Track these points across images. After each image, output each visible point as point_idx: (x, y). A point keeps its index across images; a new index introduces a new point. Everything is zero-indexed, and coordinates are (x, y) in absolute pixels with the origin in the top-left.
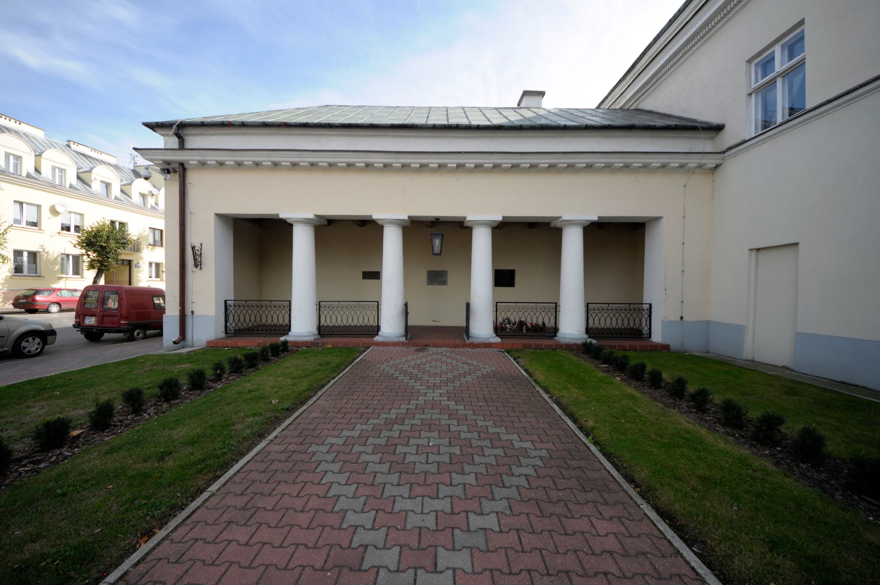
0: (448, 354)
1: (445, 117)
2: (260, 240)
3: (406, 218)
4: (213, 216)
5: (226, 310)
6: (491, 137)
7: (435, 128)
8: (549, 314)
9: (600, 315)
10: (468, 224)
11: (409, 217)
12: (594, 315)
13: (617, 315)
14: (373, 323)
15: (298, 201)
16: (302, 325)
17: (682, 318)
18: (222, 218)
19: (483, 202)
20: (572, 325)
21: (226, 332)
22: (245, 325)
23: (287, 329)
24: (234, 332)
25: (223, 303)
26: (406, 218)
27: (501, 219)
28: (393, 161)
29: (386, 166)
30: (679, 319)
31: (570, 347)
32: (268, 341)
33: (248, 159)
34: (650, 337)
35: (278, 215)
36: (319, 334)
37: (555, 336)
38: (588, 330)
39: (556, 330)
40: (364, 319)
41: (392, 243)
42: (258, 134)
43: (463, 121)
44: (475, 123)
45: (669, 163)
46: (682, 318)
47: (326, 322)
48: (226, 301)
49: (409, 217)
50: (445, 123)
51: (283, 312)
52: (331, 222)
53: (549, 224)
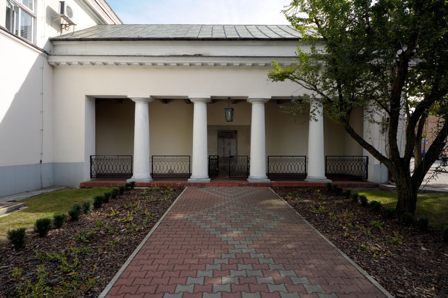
0: (229, 191)
1: (211, 33)
2: (111, 113)
3: (210, 97)
4: (84, 98)
5: (91, 161)
6: (283, 46)
7: (230, 39)
8: (302, 163)
9: (334, 164)
10: (250, 101)
11: (211, 97)
12: (330, 164)
13: (334, 164)
14: (302, 171)
15: (137, 86)
16: (141, 172)
17: (41, 161)
18: (89, 98)
19: (199, 86)
20: (316, 171)
21: (91, 177)
22: (105, 172)
23: (131, 175)
24: (98, 176)
25: (89, 157)
26: (148, 97)
27: (270, 98)
28: (184, 62)
29: (203, 65)
30: (39, 162)
31: (255, 185)
32: (120, 183)
33: (87, 61)
34: (367, 178)
35: (127, 96)
36: (152, 178)
37: (248, 178)
38: (268, 174)
39: (305, 175)
40: (178, 168)
41: (200, 114)
42: (228, 45)
43: (222, 36)
44: (229, 37)
45: (258, 63)
46: (41, 161)
47: (157, 171)
48: (91, 156)
49: (211, 97)
50: (210, 36)
51: (127, 163)
52: (166, 101)
53: (246, 100)
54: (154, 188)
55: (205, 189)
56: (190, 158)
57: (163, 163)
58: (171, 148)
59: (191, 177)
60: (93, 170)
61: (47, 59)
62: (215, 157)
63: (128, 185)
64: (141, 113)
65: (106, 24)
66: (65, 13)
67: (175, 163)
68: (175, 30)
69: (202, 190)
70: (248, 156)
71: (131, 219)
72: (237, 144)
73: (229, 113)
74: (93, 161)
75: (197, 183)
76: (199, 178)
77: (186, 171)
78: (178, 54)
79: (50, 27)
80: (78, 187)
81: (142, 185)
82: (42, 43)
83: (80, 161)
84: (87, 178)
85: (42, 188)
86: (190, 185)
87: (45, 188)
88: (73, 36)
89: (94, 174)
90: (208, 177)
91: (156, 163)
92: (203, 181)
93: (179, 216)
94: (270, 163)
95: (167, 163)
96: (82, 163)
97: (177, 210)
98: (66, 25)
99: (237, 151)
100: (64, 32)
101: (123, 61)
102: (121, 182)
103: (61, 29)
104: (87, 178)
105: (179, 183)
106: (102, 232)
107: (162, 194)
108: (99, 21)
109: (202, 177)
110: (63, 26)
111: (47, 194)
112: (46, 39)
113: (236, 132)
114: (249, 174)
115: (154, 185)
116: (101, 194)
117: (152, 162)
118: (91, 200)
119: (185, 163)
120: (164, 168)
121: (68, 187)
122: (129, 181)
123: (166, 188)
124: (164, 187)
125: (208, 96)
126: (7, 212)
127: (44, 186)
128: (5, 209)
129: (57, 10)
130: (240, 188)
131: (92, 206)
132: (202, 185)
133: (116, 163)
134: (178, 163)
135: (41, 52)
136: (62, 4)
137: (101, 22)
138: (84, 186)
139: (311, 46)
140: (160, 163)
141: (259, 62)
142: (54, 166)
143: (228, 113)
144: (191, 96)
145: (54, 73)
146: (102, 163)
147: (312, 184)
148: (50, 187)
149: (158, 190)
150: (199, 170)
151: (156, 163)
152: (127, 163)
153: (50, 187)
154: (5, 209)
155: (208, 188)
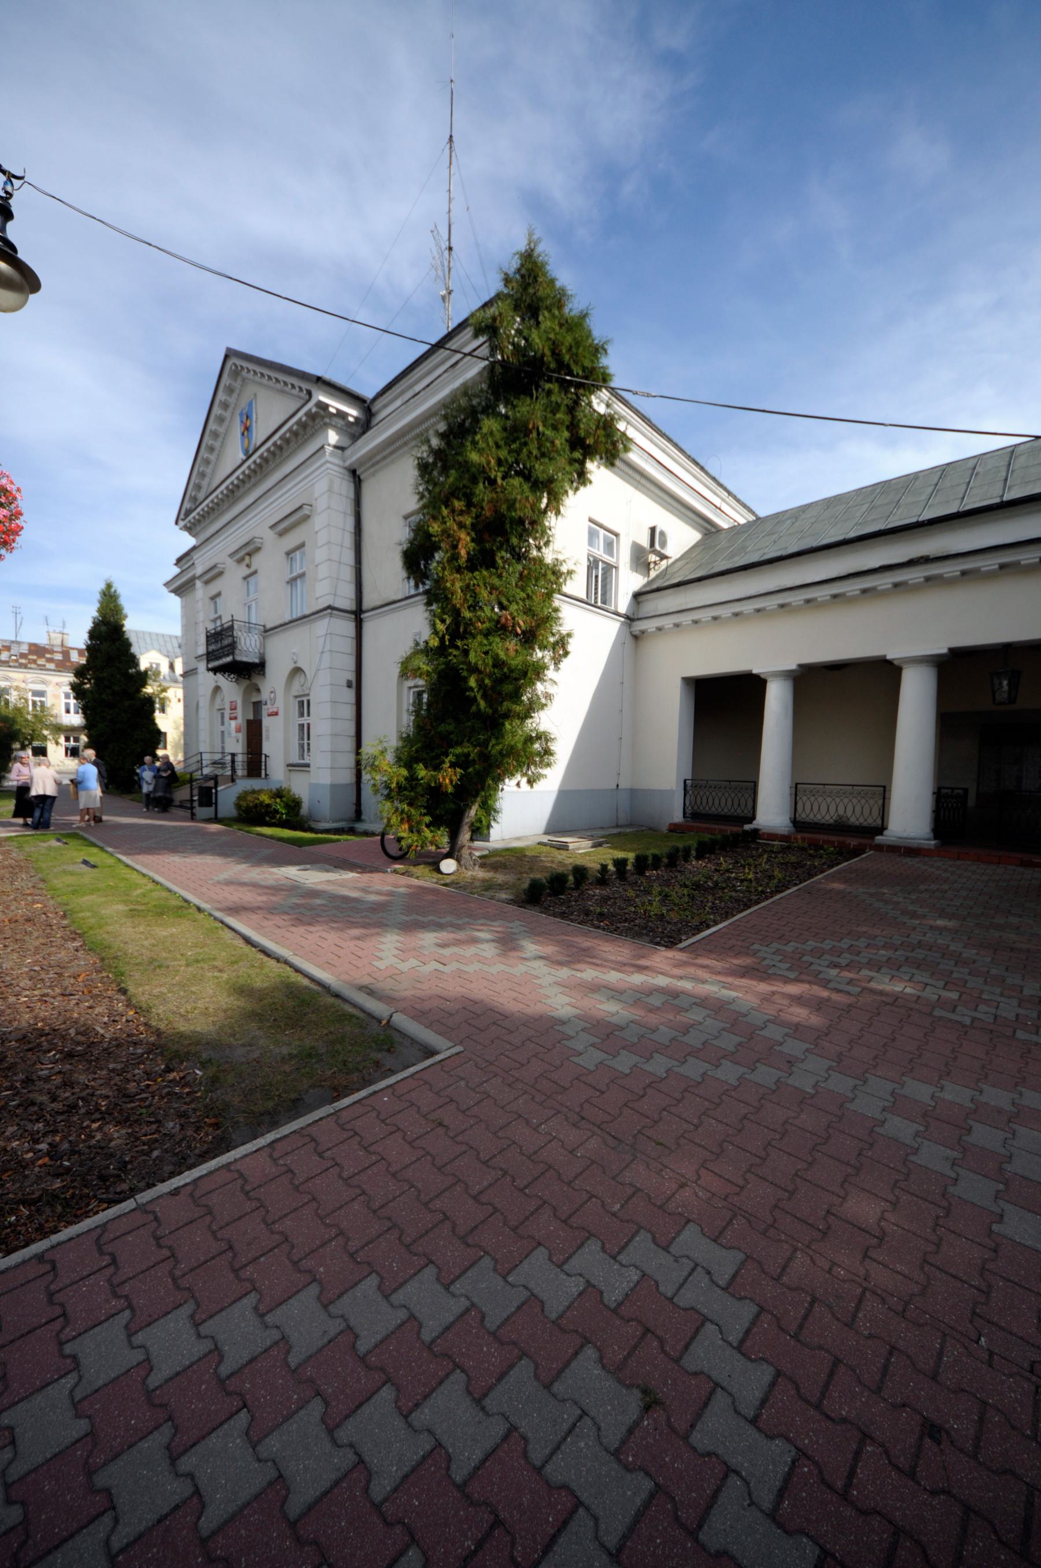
2: (724, 705)
5: (685, 789)
15: (770, 649)
16: (772, 812)
24: (695, 815)
26: (794, 667)
32: (731, 829)
33: (686, 619)
48: (685, 781)
51: (747, 795)
54: (795, 845)
55: (917, 859)
56: (884, 792)
57: (820, 799)
58: (841, 767)
59: (885, 832)
60: (687, 804)
61: (630, 626)
62: (956, 791)
63: (746, 832)
64: (777, 701)
65: (719, 530)
66: (657, 547)
67: (846, 801)
68: (866, 506)
69: (908, 860)
71: (751, 876)
74: (688, 788)
76: (905, 835)
77: (873, 820)
78: (865, 568)
79: (635, 574)
80: (665, 829)
81: (772, 836)
82: (623, 603)
84: (678, 817)
85: (617, 826)
86: (879, 848)
87: (621, 827)
88: (667, 577)
89: (689, 811)
90: (931, 835)
91: (805, 798)
93: (836, 886)
95: (829, 800)
96: (672, 791)
97: (833, 878)
98: (655, 562)
100: (653, 574)
101: (748, 607)
102: (735, 829)
103: (649, 570)
104: (678, 817)
105: (853, 842)
106: (710, 884)
107: (810, 855)
108: (706, 529)
109: (913, 835)
110: (652, 565)
111: (626, 834)
112: (630, 596)
115: (796, 839)
116: (707, 837)
117: (796, 795)
118: (693, 843)
119: (872, 802)
120: (824, 810)
121: (650, 829)
122: (747, 827)
123: (822, 848)
124: (816, 846)
125: (941, 648)
126: (592, 847)
127: (621, 822)
128: (590, 843)
129: (645, 543)
130: (1021, 869)
131: (693, 853)
132: (907, 851)
133: (727, 794)
135: (622, 619)
136: (653, 530)
137: (709, 529)
138: (674, 828)
140: (812, 799)
142: (633, 792)
143: (1001, 684)
145: (637, 646)
146: (702, 793)
148: (627, 826)
149: (803, 849)
151: (805, 798)
152: (747, 795)
153: (627, 826)
154: (590, 843)
155: (926, 859)
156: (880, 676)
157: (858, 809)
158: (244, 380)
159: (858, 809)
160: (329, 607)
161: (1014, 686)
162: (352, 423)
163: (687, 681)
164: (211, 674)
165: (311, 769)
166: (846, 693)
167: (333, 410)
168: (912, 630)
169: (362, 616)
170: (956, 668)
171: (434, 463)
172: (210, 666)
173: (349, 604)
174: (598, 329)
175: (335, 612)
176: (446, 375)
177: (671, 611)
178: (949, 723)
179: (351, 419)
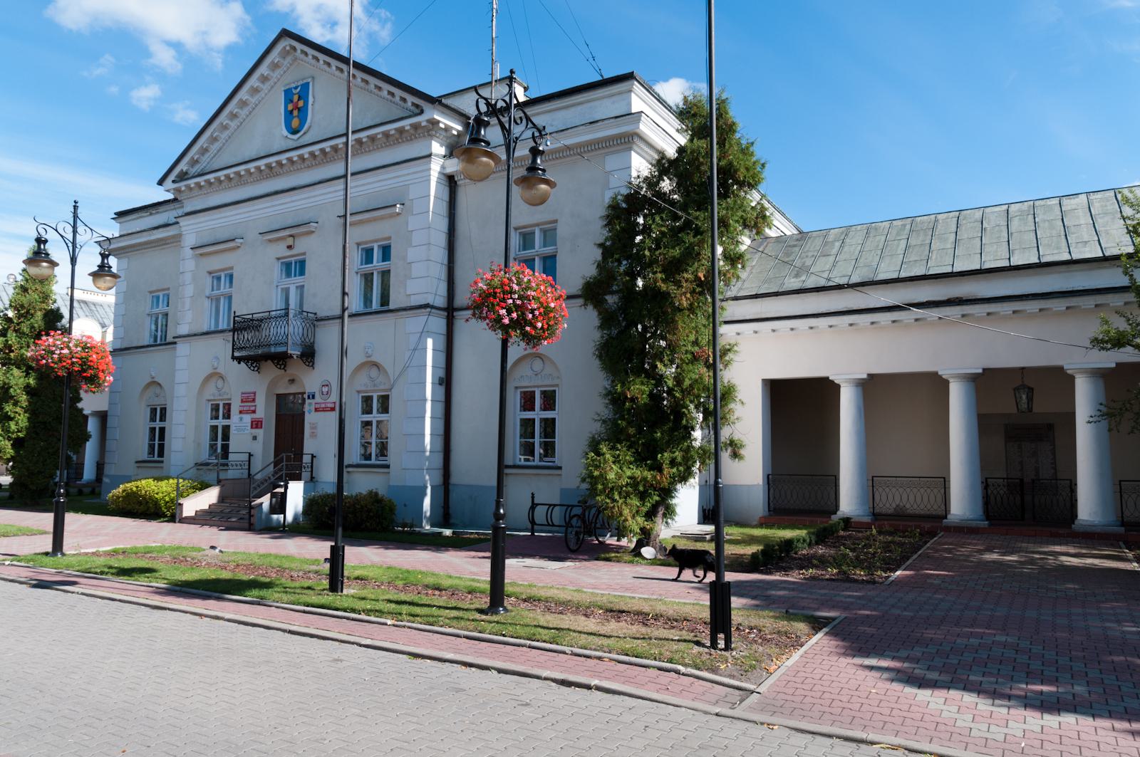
4: (759, 385)
6: (1100, 268)
16: (849, 501)
21: (769, 511)
41: (958, 398)
57: (894, 490)
60: (771, 496)
70: (1071, 480)
72: (1054, 454)
73: (1024, 397)
75: (963, 528)
83: (756, 483)
90: (984, 517)
91: (880, 490)
92: (974, 524)
94: (1125, 496)
99: (1055, 469)
113: (1050, 427)
114: (1077, 516)
120: (890, 501)
132: (964, 530)
134: (922, 490)
139: (678, 317)
140: (887, 490)
141: (1027, 308)
143: (1021, 397)
144: (1069, 366)
147: (1082, 530)
150: (961, 501)
151: (880, 490)
156: (934, 385)
157: (912, 498)
158: (296, 59)
159: (912, 498)
160: (426, 306)
161: (1030, 400)
162: (454, 135)
163: (764, 381)
164: (235, 362)
165: (563, 472)
166: (901, 398)
167: (442, 126)
168: (954, 351)
169: (455, 314)
170: (985, 383)
171: (644, 238)
172: (236, 354)
173: (441, 301)
174: (759, 152)
175: (433, 311)
176: (584, 127)
177: (748, 318)
178: (984, 423)
179: (455, 133)
